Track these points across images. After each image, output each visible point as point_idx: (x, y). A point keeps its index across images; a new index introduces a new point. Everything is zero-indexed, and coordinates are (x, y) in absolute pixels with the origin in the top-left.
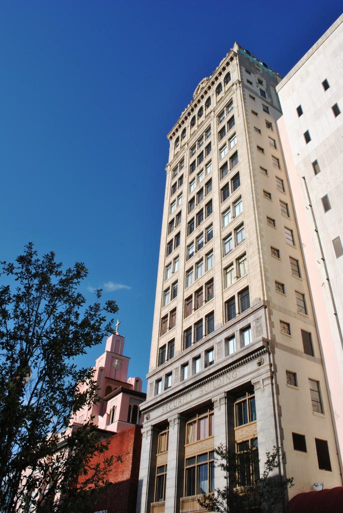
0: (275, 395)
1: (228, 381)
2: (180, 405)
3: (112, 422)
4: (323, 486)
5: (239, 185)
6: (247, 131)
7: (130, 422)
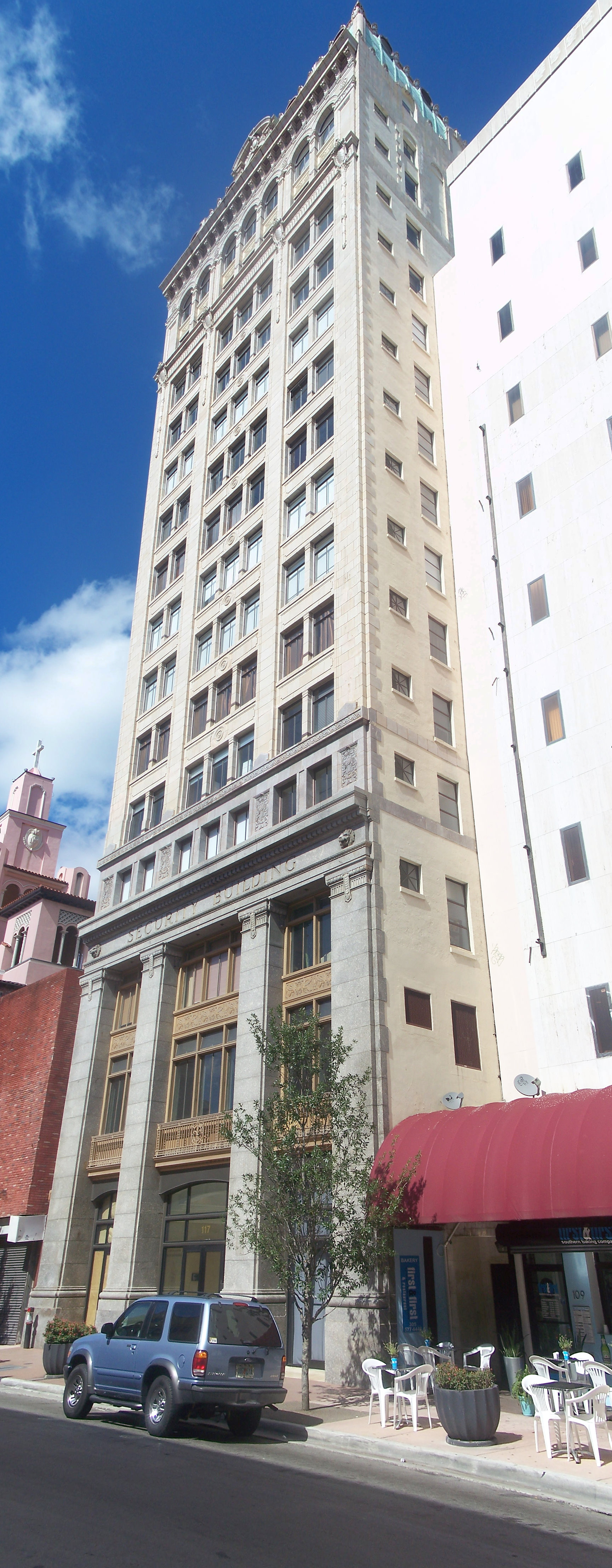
0: (374, 910)
3: (17, 962)
4: (462, 1099)
5: (331, 433)
6: (361, 290)
7: (59, 962)
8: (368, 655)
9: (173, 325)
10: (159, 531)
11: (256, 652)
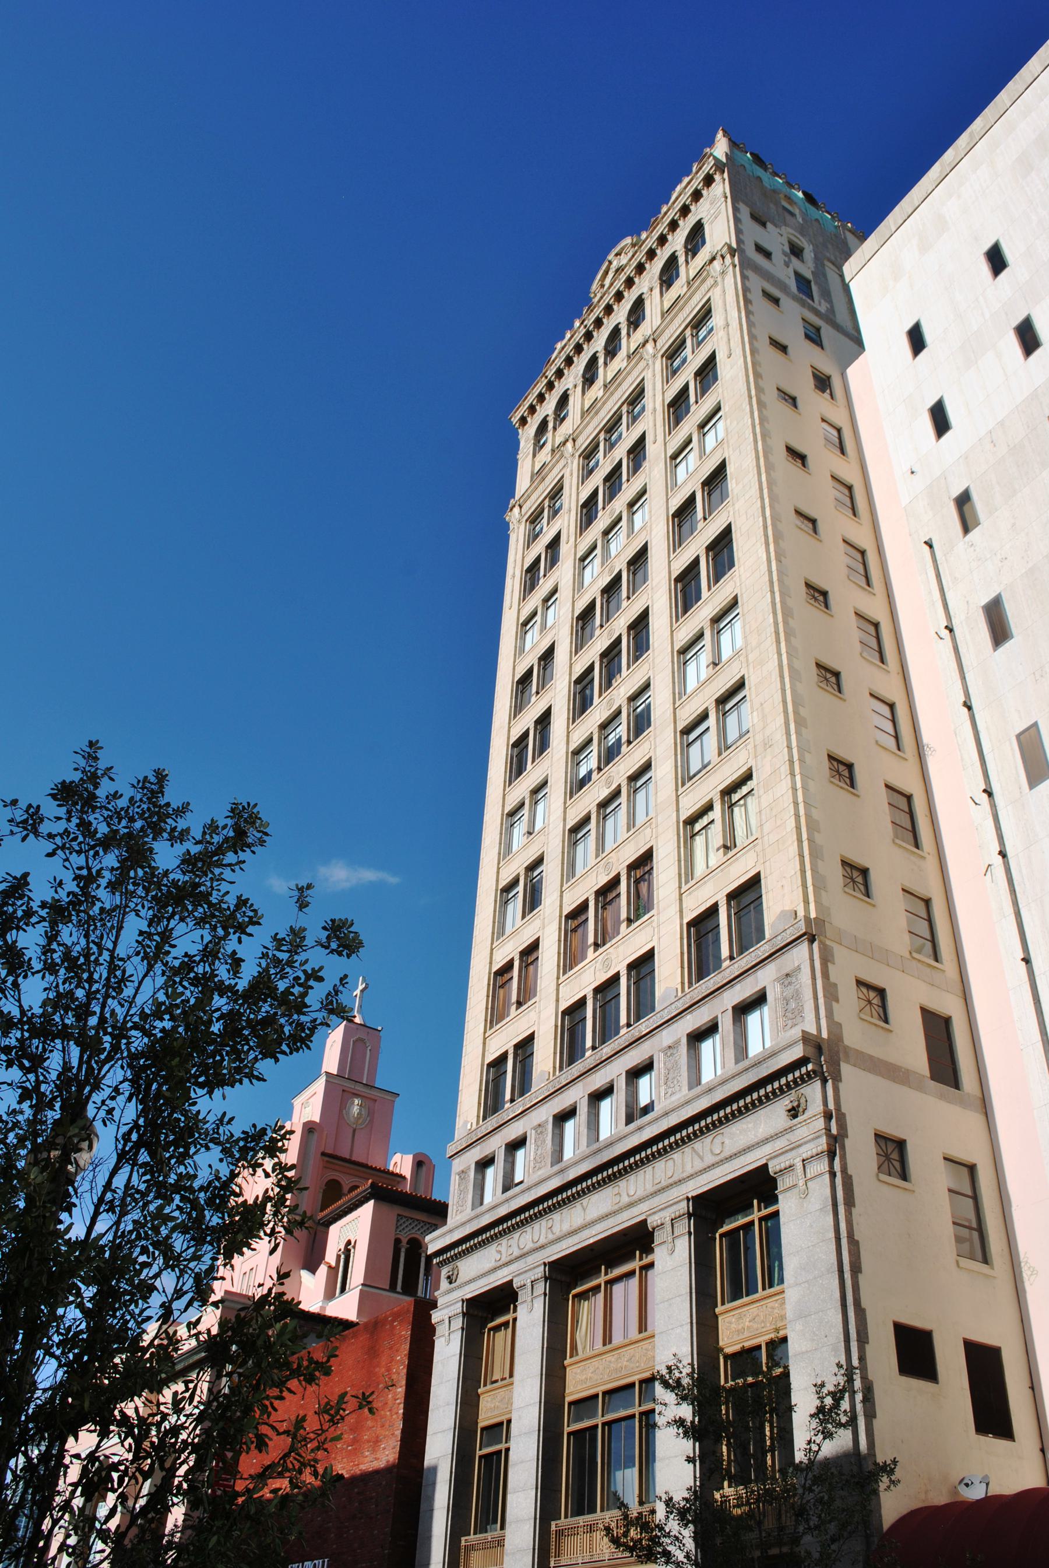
1: (699, 1165)
2: (551, 1237)
3: (343, 1290)
4: (987, 1484)
5: (732, 565)
6: (754, 400)
8: (805, 844)
9: (526, 457)
10: (516, 698)
11: (652, 848)
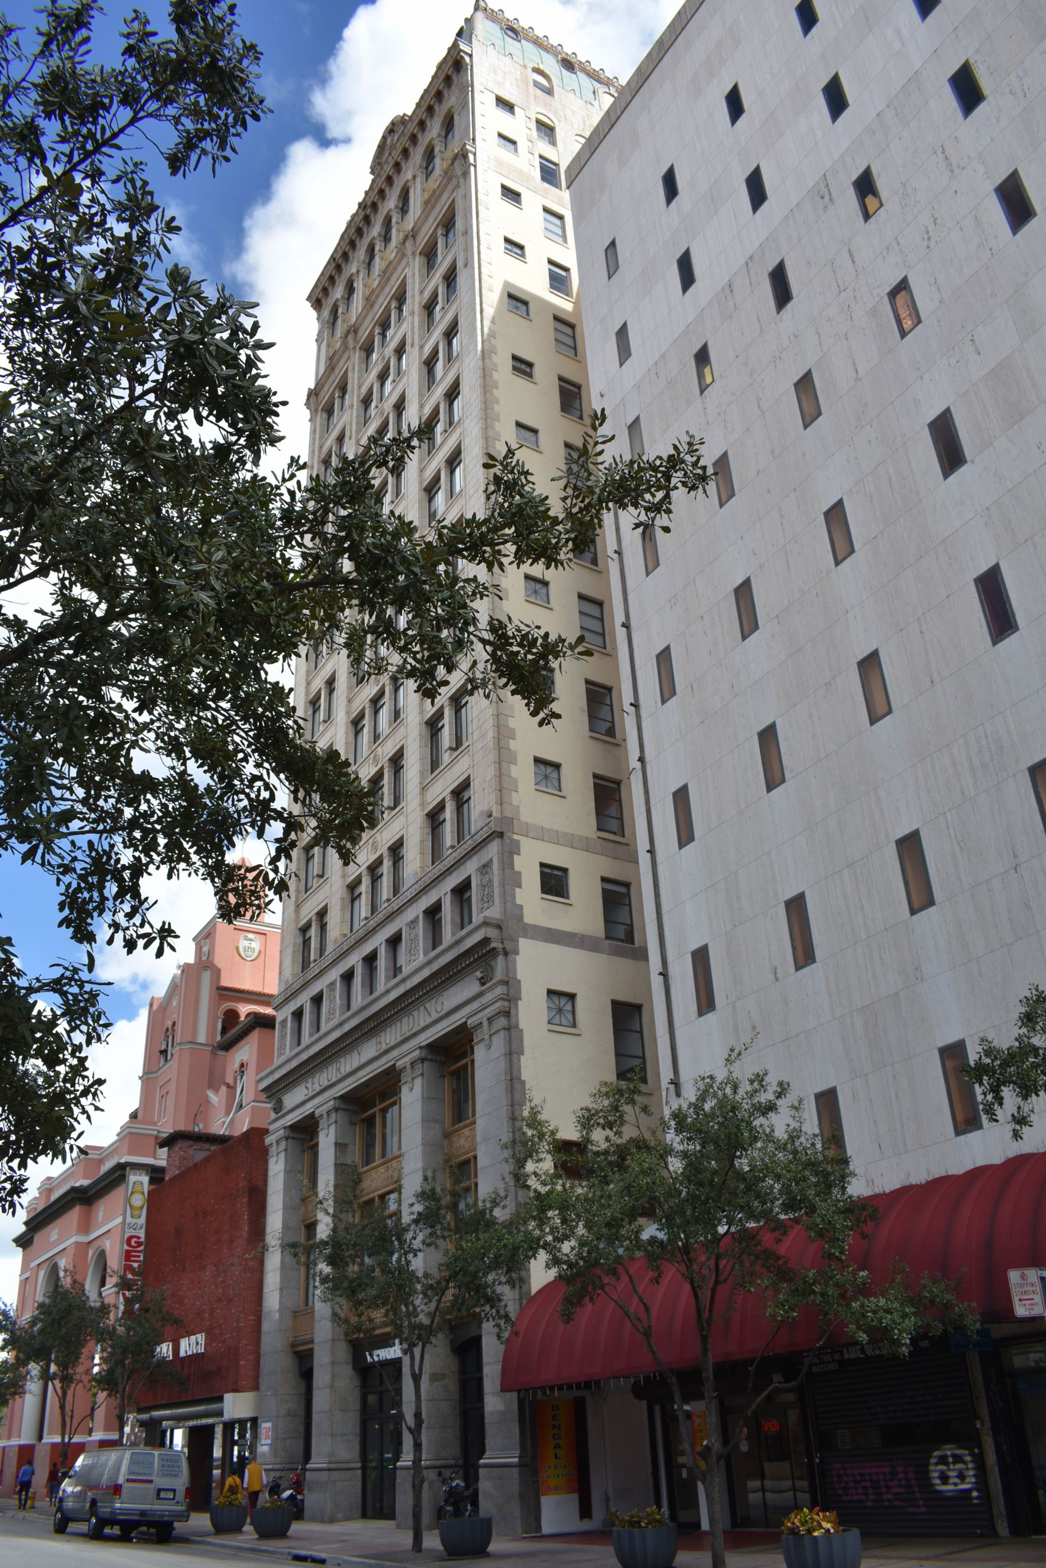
1: (429, 1020)
2: (339, 1076)
